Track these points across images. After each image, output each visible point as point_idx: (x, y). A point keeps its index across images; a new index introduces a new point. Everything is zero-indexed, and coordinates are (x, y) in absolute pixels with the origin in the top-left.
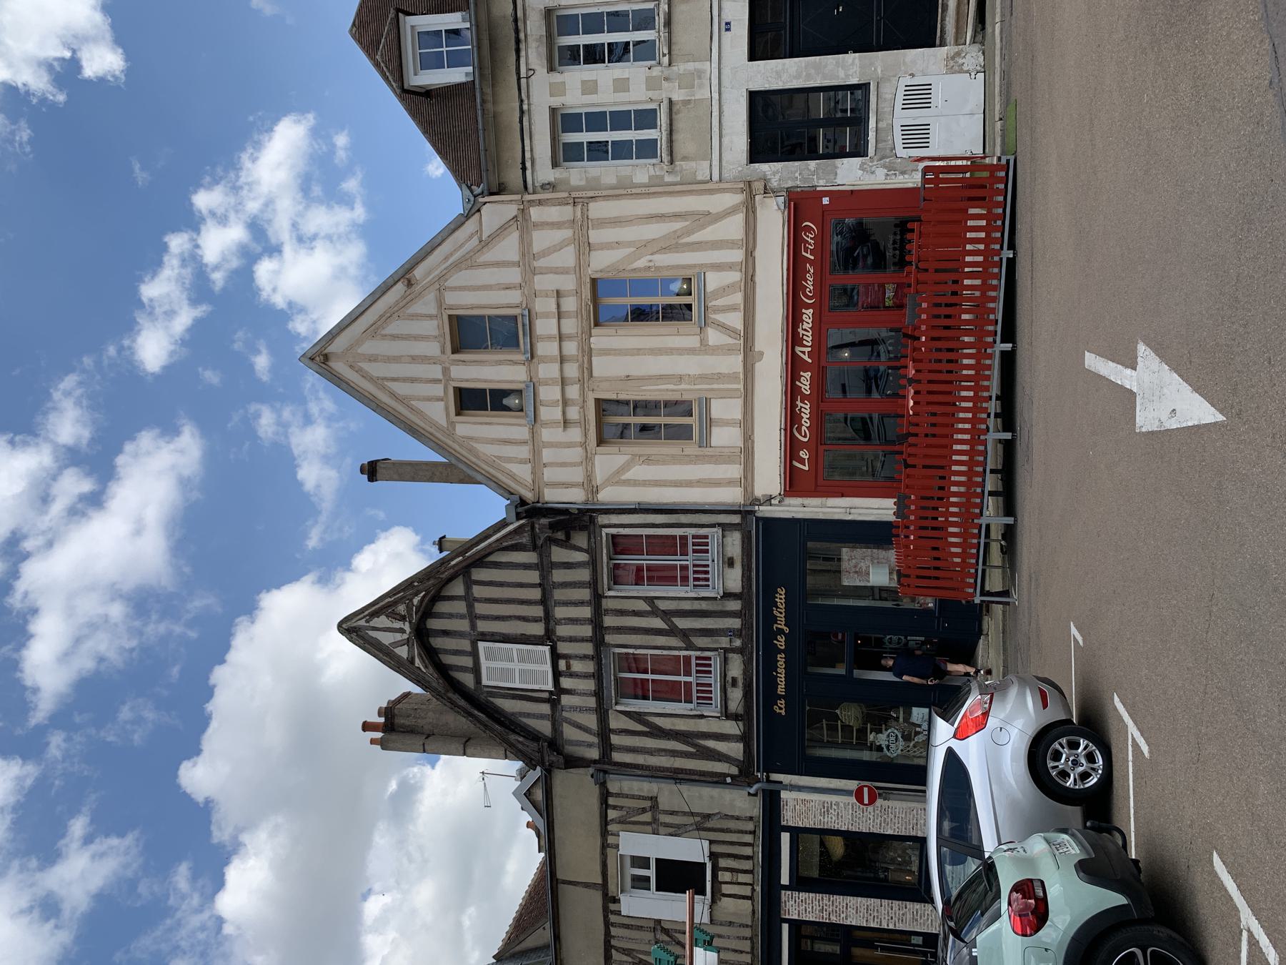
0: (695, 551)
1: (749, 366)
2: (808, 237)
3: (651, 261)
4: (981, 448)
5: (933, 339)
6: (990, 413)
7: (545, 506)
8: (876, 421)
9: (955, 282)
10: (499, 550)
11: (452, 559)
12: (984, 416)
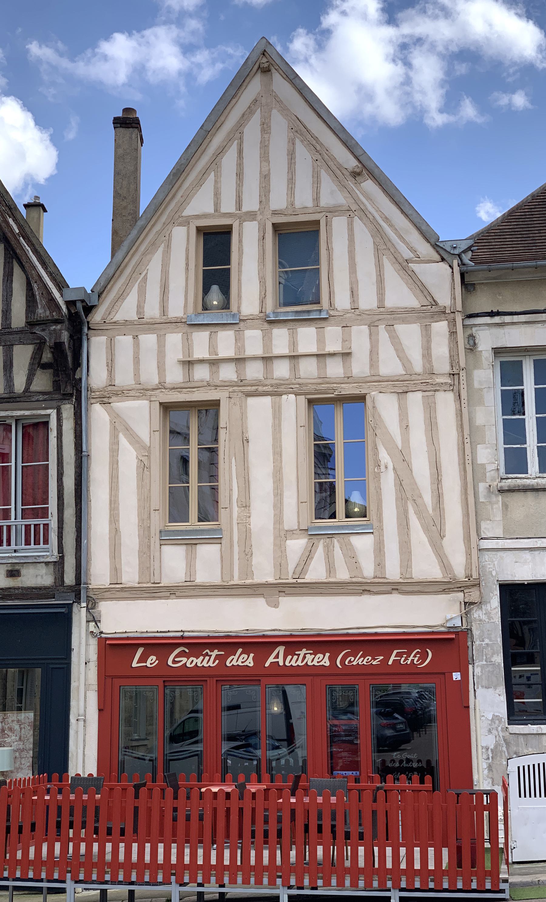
0: (28, 527)
1: (261, 590)
2: (415, 656)
3: (386, 467)
4: (160, 878)
5: (293, 812)
6: (203, 886)
7: (85, 338)
8: (194, 748)
9: (361, 836)
10: (28, 279)
11: (15, 220)
12: (200, 880)
